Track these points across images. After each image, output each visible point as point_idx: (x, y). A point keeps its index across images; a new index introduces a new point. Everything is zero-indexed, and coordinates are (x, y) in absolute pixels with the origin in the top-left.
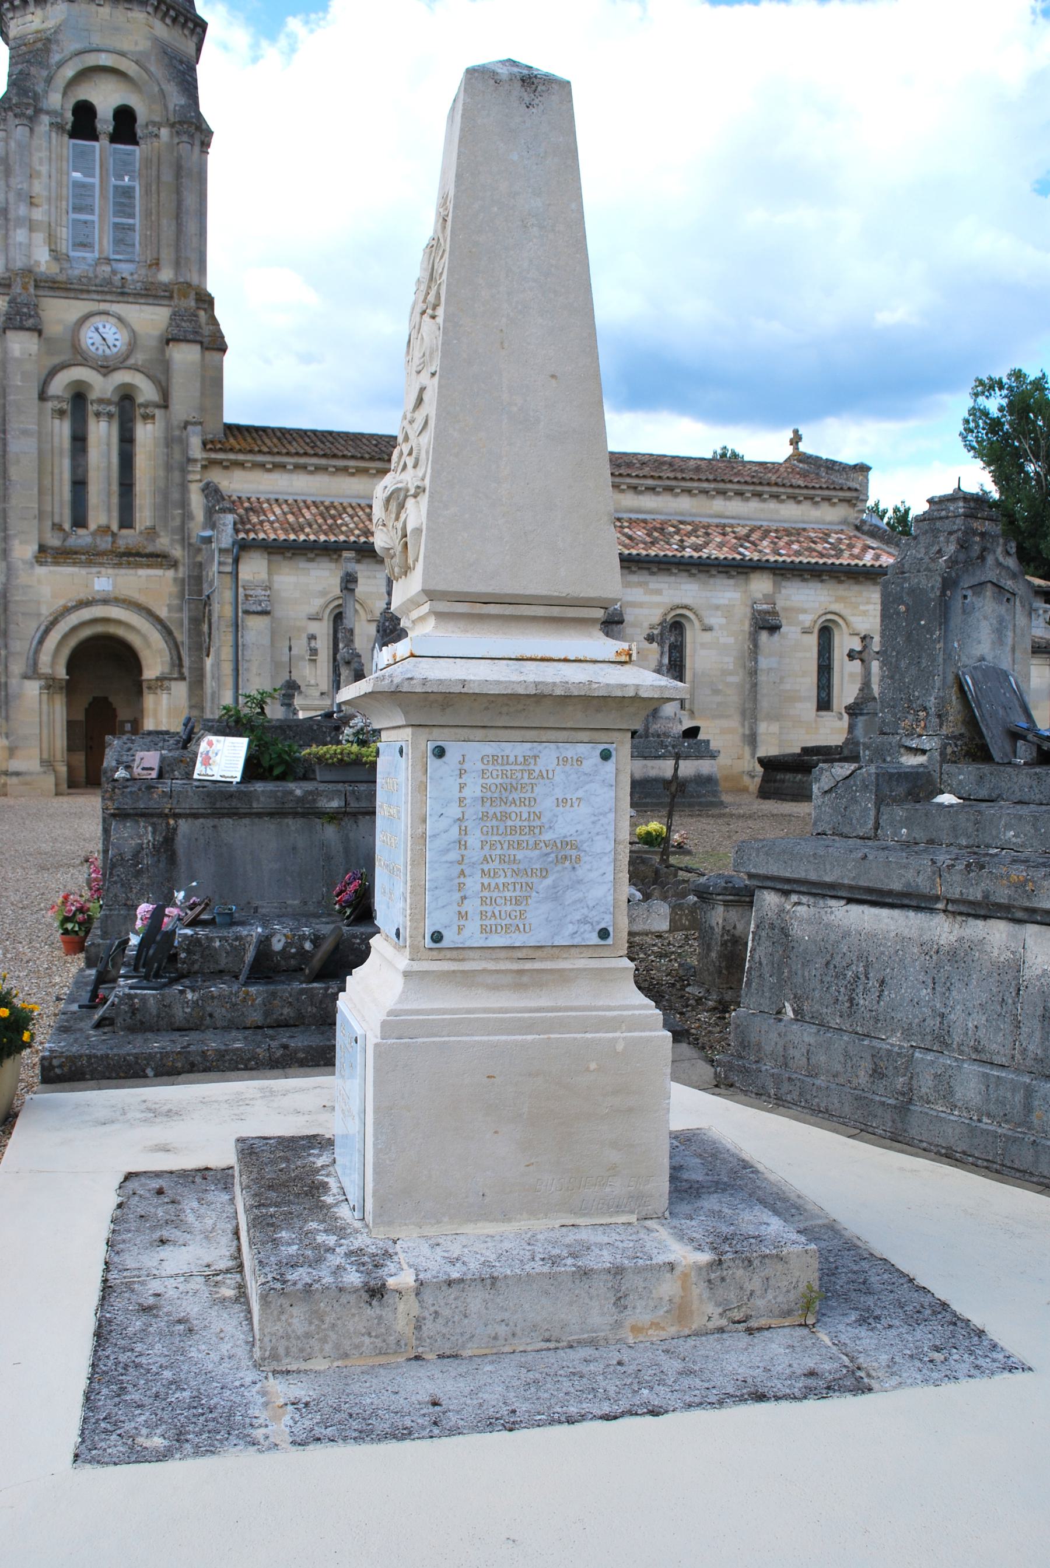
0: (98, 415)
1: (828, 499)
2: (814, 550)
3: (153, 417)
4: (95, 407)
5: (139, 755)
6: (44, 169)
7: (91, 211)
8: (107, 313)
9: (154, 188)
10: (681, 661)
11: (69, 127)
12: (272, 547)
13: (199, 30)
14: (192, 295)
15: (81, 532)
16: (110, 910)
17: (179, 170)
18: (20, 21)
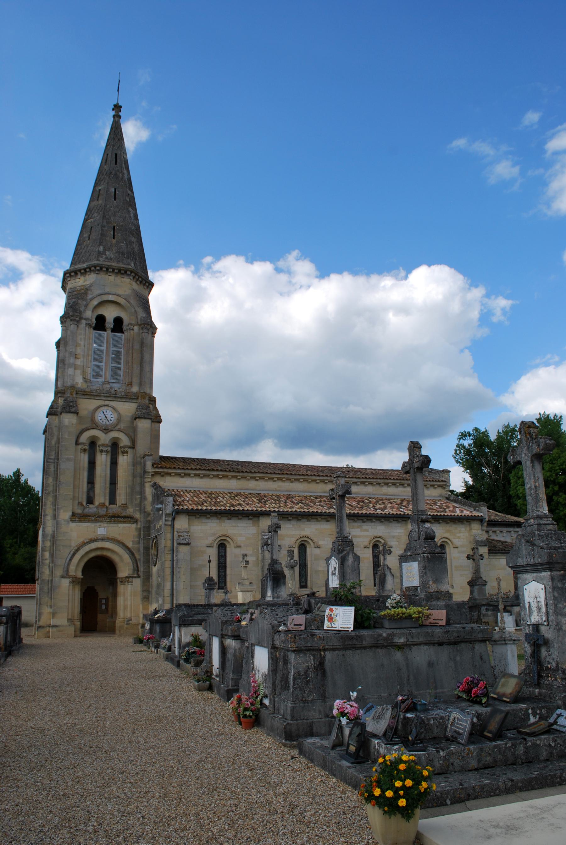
0: (101, 451)
1: (432, 486)
2: (433, 509)
3: (127, 452)
4: (101, 448)
5: (290, 618)
6: (82, 343)
7: (102, 361)
8: (108, 406)
9: (130, 351)
10: (378, 563)
11: (93, 325)
12: (190, 513)
13: (150, 286)
14: (147, 398)
15: (91, 506)
16: (295, 704)
17: (142, 344)
18: (73, 281)
